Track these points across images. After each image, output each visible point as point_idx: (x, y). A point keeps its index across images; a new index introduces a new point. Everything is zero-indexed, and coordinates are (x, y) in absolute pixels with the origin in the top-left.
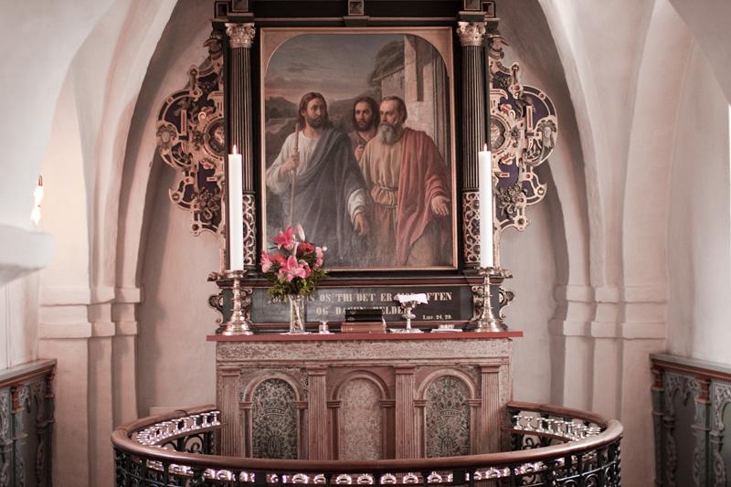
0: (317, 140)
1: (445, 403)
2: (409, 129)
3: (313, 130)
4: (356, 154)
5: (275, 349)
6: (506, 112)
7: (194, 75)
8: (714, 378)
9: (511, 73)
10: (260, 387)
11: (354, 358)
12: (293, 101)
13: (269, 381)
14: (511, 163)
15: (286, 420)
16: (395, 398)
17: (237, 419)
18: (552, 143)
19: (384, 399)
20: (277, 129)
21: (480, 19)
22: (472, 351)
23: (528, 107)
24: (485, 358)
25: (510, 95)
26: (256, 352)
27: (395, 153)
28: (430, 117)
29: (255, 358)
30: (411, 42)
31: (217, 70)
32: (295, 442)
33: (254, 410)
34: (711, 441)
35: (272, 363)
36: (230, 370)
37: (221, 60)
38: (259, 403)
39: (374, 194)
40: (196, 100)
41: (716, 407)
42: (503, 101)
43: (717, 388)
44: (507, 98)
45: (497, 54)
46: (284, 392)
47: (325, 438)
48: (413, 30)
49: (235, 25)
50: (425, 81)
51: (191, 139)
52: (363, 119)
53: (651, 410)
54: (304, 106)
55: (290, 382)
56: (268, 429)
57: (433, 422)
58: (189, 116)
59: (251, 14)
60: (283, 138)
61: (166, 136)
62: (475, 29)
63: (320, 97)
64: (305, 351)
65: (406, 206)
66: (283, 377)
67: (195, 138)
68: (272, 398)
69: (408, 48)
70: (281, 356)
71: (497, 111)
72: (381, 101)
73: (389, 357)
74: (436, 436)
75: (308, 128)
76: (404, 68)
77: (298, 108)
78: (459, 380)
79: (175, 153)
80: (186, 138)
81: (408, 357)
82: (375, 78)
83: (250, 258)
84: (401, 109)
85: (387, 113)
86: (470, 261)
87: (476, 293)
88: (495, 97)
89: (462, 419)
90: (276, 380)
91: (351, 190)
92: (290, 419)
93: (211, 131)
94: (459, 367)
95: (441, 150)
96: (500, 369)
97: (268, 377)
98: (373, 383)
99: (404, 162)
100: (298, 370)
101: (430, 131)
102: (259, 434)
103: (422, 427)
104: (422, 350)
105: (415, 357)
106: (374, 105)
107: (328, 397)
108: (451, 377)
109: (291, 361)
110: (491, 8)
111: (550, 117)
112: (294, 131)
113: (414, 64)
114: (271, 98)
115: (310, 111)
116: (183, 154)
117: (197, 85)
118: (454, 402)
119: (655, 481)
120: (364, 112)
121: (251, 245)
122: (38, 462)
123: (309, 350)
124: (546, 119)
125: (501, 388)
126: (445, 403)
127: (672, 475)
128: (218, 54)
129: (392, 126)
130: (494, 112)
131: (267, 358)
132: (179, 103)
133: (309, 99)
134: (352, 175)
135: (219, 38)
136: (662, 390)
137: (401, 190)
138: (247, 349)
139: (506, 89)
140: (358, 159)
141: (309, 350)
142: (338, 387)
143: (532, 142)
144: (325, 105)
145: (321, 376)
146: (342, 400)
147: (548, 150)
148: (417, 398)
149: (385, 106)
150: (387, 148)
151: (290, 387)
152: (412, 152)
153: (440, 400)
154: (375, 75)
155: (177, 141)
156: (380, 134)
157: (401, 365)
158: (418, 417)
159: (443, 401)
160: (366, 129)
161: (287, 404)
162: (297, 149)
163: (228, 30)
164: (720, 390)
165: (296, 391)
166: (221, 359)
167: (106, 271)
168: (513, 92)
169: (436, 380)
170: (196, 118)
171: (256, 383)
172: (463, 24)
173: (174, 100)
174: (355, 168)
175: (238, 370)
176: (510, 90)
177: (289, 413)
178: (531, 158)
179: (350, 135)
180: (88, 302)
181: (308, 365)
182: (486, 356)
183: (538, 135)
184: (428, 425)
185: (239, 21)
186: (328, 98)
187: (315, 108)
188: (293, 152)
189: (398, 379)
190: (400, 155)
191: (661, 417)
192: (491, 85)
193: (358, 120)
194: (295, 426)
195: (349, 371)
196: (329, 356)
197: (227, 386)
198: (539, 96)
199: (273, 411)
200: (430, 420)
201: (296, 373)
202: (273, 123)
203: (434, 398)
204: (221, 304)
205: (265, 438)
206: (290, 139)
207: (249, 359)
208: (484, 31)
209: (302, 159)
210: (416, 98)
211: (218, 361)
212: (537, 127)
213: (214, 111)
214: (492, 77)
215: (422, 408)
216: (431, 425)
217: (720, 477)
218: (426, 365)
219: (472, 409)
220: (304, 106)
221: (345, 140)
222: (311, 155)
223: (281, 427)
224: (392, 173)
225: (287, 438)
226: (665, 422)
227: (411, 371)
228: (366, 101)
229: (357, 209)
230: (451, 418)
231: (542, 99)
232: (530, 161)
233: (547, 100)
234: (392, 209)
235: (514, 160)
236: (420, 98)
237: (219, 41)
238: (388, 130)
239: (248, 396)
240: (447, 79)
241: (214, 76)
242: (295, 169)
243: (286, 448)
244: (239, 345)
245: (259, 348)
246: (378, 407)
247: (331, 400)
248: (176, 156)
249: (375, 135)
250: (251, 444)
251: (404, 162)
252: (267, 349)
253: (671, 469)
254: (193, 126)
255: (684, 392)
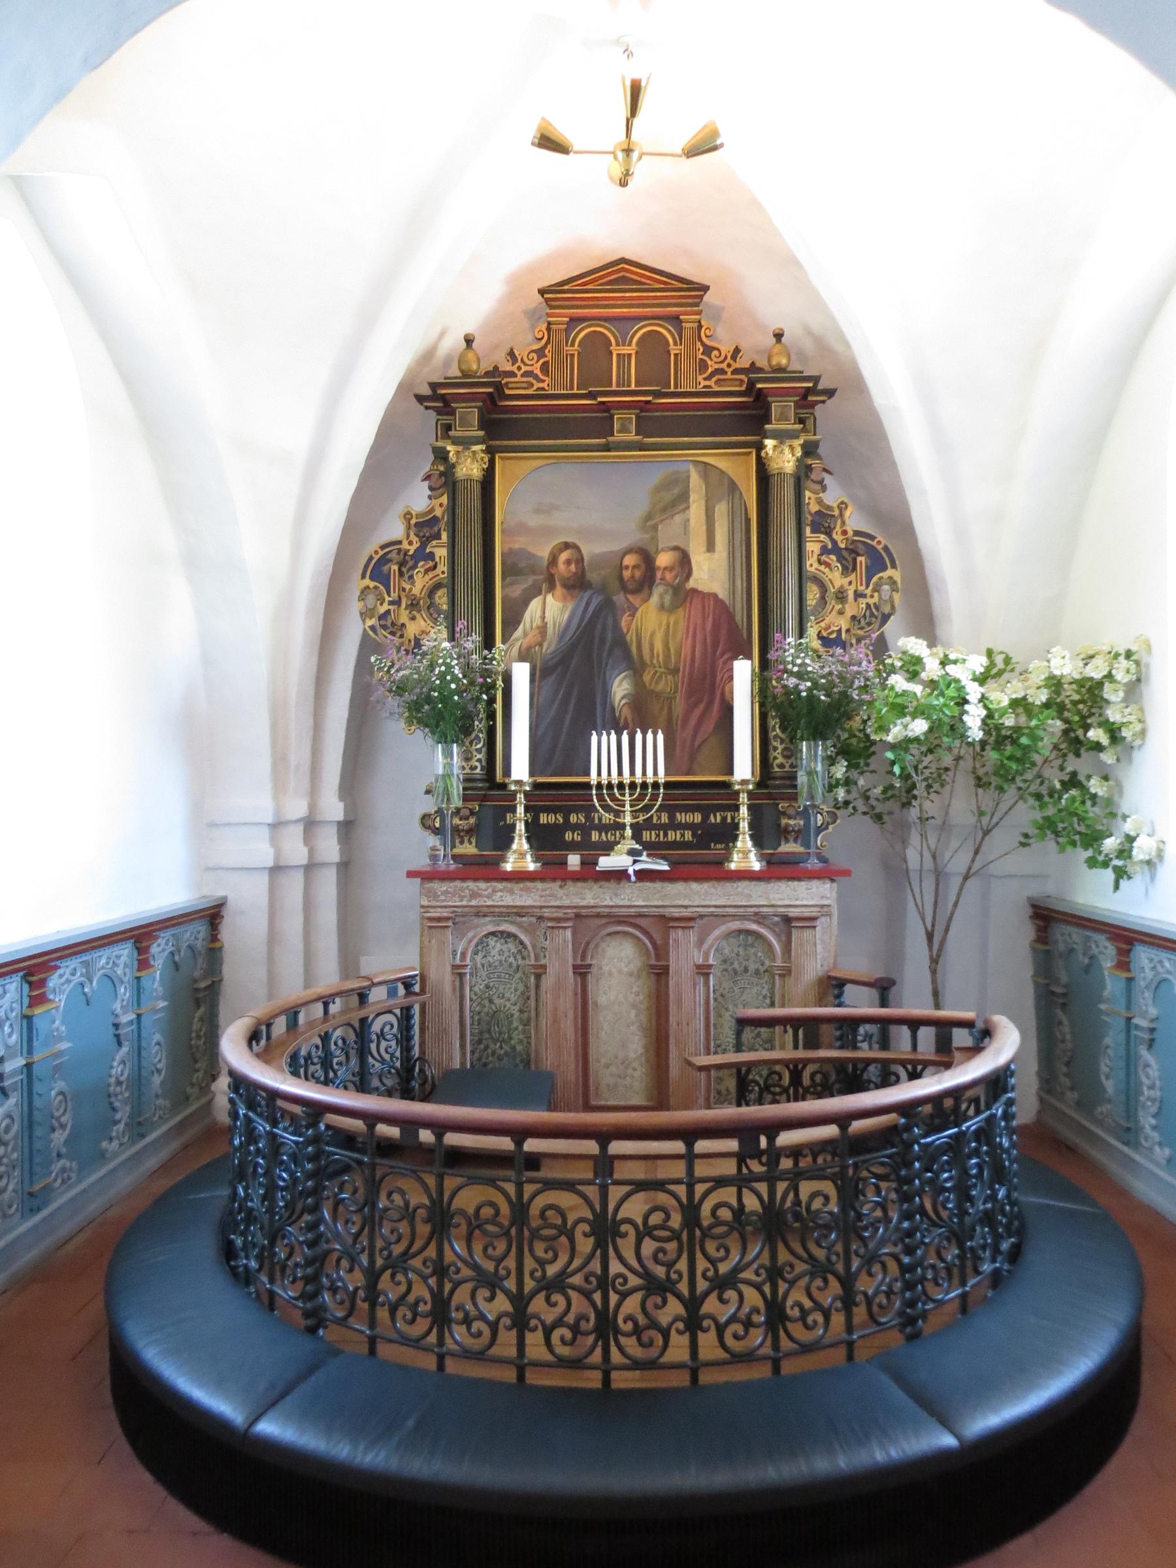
0: (570, 606)
1: (740, 969)
2: (694, 591)
3: (564, 591)
4: (623, 624)
5: (501, 891)
6: (828, 565)
7: (410, 520)
8: (1137, 940)
9: (836, 513)
10: (480, 942)
11: (612, 904)
12: (539, 554)
13: (493, 934)
14: (834, 636)
15: (516, 990)
16: (668, 961)
17: (448, 988)
18: (893, 607)
19: (653, 962)
20: (516, 591)
21: (794, 435)
22: (777, 896)
23: (859, 559)
24: (796, 906)
25: (834, 542)
26: (474, 895)
27: (676, 623)
28: (722, 574)
29: (473, 903)
30: (699, 472)
31: (438, 512)
32: (529, 1020)
33: (471, 974)
34: (1134, 1032)
35: (497, 910)
36: (439, 919)
37: (444, 499)
38: (479, 965)
39: (647, 678)
40: (411, 553)
41: (1143, 984)
42: (824, 550)
43: (1143, 956)
44: (830, 546)
45: (817, 487)
46: (514, 950)
47: (571, 1014)
48: (704, 455)
49: (460, 448)
50: (717, 524)
51: (403, 605)
52: (633, 577)
53: (1031, 973)
54: (553, 561)
55: (523, 937)
56: (491, 1001)
57: (722, 995)
58: (401, 574)
59: (481, 433)
60: (526, 603)
61: (371, 600)
62: (787, 450)
63: (576, 548)
64: (544, 893)
65: (690, 694)
66: (512, 929)
67: (409, 602)
68: (497, 957)
69: (695, 480)
70: (509, 900)
71: (816, 565)
72: (657, 552)
73: (660, 903)
74: (728, 1014)
75: (559, 590)
76: (688, 507)
77: (546, 563)
78: (758, 936)
79: (382, 622)
80: (397, 603)
81: (686, 903)
82: (649, 523)
83: (477, 764)
84: (684, 562)
85: (665, 569)
86: (776, 769)
87: (784, 814)
88: (812, 548)
89: (765, 992)
90: (502, 932)
91: (616, 672)
92: (521, 987)
93: (432, 593)
94: (759, 918)
95: (738, 618)
96: (818, 923)
97: (491, 928)
98: (638, 938)
99: (687, 637)
100: (533, 920)
101: (722, 594)
102: (478, 1009)
103: (707, 1003)
104: (706, 893)
105: (696, 903)
106: (648, 559)
107: (575, 958)
108: (749, 932)
109: (523, 907)
110: (809, 423)
111: (890, 572)
112: (539, 593)
113: (703, 502)
114: (510, 549)
115: (561, 566)
116: (393, 624)
117: (412, 534)
118: (752, 967)
119: (1038, 1073)
120: (634, 567)
121: (479, 746)
122: (194, 1035)
123: (548, 892)
124: (885, 574)
125: (819, 948)
126: (740, 969)
127: (1064, 1069)
128: (440, 491)
129: (672, 587)
130: (811, 565)
131: (489, 903)
132: (389, 556)
133: (561, 551)
134: (618, 652)
135: (442, 468)
136: (1047, 948)
137: (684, 672)
138: (462, 889)
139: (828, 533)
140: (625, 631)
141: (548, 892)
142: (588, 943)
143: (864, 606)
144: (582, 559)
145: (565, 928)
146: (594, 962)
147: (885, 618)
148: (701, 961)
149: (664, 560)
150: (664, 617)
151: (522, 943)
152: (699, 622)
153: (732, 964)
154: (649, 517)
155: (385, 607)
156: (655, 599)
157: (677, 915)
158: (701, 988)
159: (736, 965)
160: (637, 591)
161: (518, 967)
162: (543, 617)
163: (451, 454)
164: (1151, 960)
165: (530, 947)
166: (425, 903)
167: (298, 781)
168: (838, 537)
169: (729, 935)
170: (411, 577)
171: (474, 937)
172: (769, 443)
173: (381, 553)
174: (620, 642)
175: (447, 919)
176: (834, 536)
177: (521, 979)
178: (862, 628)
179: (615, 598)
180: (270, 821)
181: (547, 913)
182: (798, 903)
183: (872, 596)
184: (715, 1000)
185: (465, 443)
186: (586, 550)
187: (568, 562)
188: (537, 622)
189: (673, 934)
190: (682, 625)
191: (1048, 985)
192: (808, 530)
193: (626, 579)
194: (528, 998)
195: (604, 921)
196: (577, 901)
197: (434, 941)
198: (874, 543)
199: (499, 977)
200: (718, 994)
201: (531, 924)
202: (512, 584)
203: (725, 961)
204: (437, 825)
205: (487, 1014)
206: (535, 605)
207: (464, 903)
208: (799, 452)
209: (550, 631)
210: (704, 549)
211: (422, 907)
212: (871, 587)
213: (435, 567)
214: (810, 518)
215: (708, 975)
216: (720, 999)
217: (1151, 1087)
218: (712, 915)
219: (777, 977)
220: (553, 561)
221: (608, 605)
222: (563, 625)
223: (509, 999)
224: (672, 651)
225: (517, 1014)
226: (1053, 993)
227: (691, 924)
228: (636, 552)
229: (623, 698)
230: (748, 990)
231: (879, 548)
232: (860, 632)
233: (886, 548)
234: (670, 699)
235: (839, 631)
236: (711, 547)
237: (442, 474)
238: (666, 592)
239: (463, 955)
240: (748, 521)
241: (435, 520)
242: (541, 645)
243: (516, 1029)
244: (452, 884)
245: (479, 889)
246: (644, 973)
247: (579, 962)
248: (384, 627)
249: (648, 599)
250: (468, 1021)
251: (687, 637)
252: (490, 890)
253: (1066, 1059)
254: (407, 587)
255: (1084, 954)
